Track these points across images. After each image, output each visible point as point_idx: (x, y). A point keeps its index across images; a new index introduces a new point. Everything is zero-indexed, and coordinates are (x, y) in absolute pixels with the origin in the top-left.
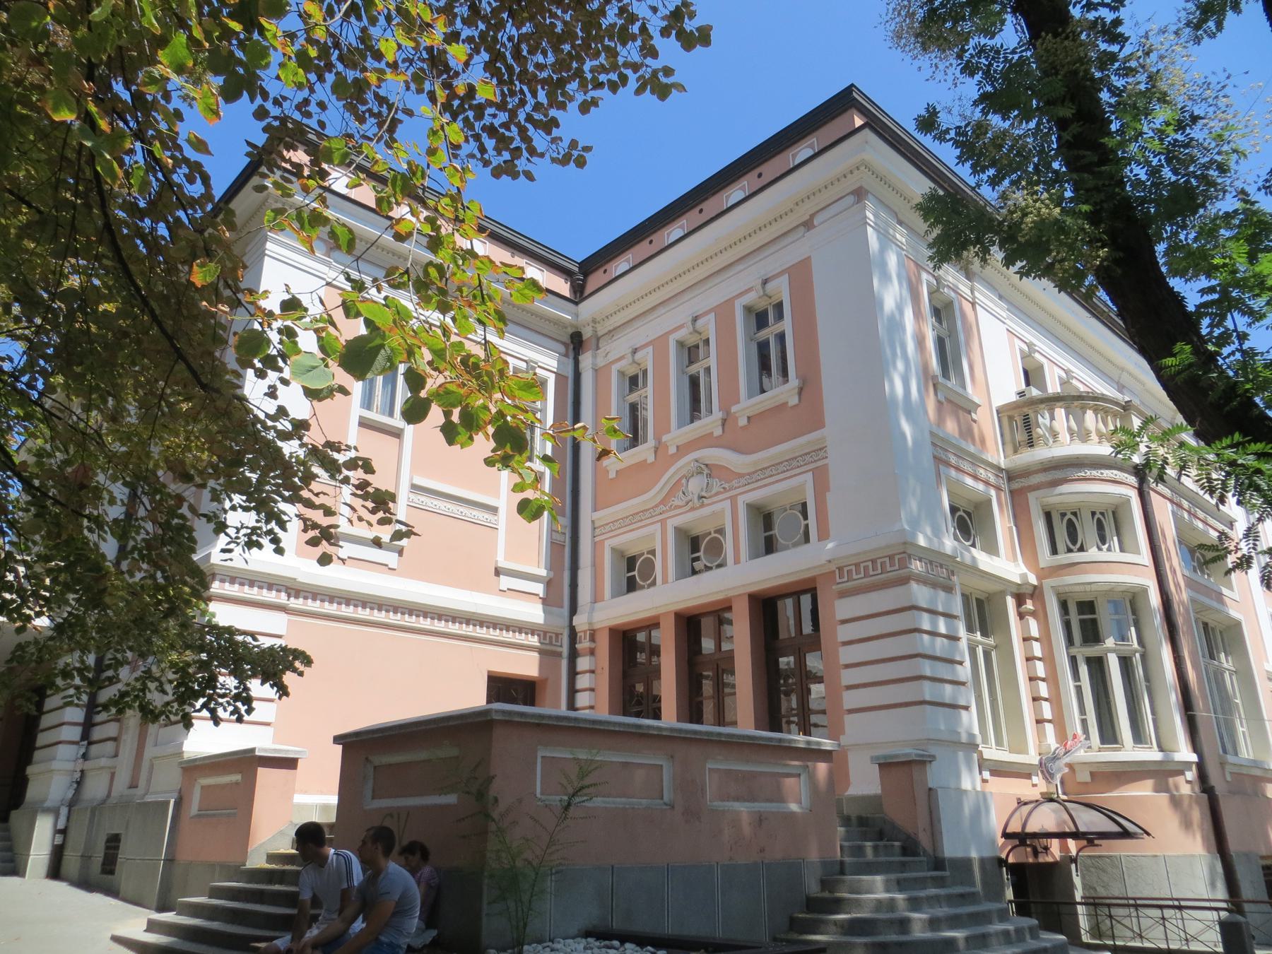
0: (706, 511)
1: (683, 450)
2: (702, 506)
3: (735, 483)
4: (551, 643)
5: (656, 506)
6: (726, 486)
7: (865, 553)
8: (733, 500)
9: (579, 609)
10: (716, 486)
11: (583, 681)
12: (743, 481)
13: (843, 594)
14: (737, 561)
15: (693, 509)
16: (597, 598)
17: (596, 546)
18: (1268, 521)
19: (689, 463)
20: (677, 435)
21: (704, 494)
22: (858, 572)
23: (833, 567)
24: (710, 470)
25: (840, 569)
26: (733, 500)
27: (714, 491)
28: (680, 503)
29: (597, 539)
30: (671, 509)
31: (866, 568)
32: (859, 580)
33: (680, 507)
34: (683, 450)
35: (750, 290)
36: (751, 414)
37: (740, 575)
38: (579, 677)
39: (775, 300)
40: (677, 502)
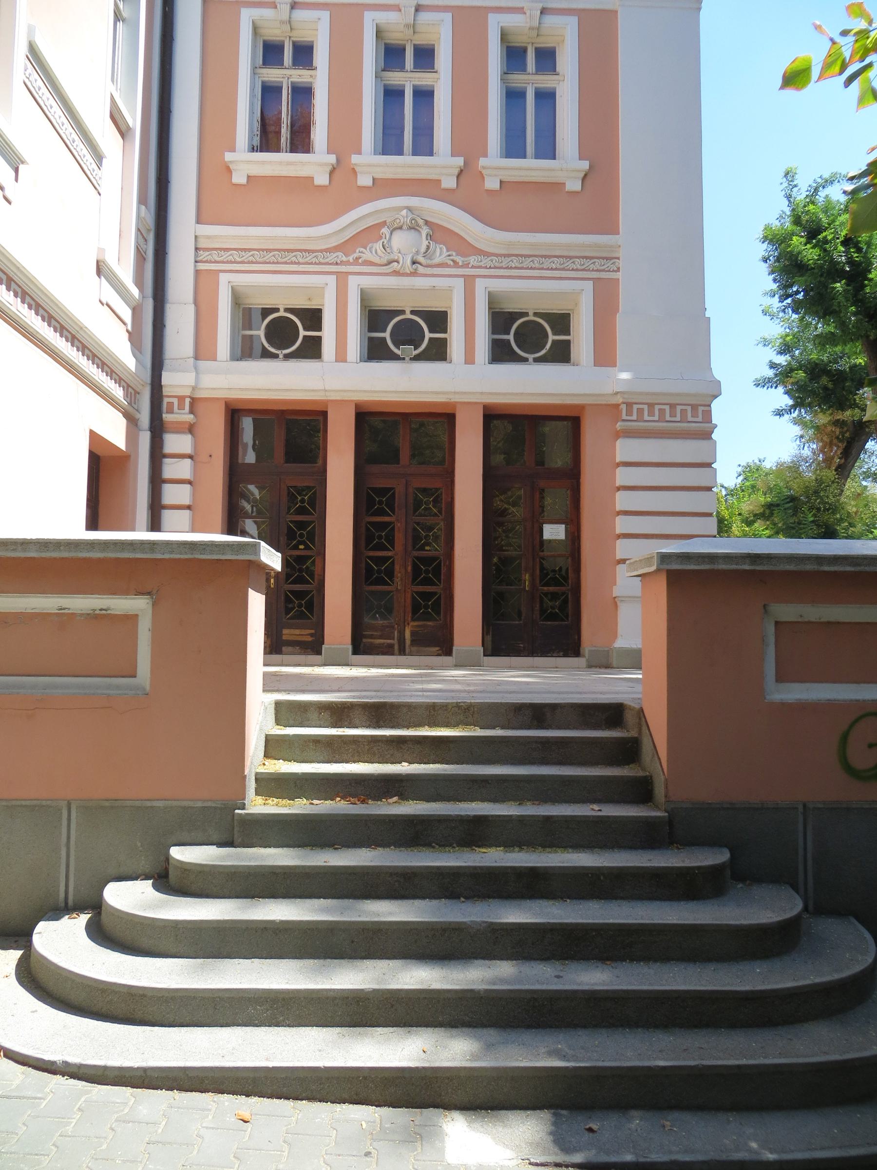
0: (419, 282)
1: (384, 187)
2: (414, 274)
3: (473, 260)
4: (661, 419)
5: (327, 250)
6: (459, 260)
7: (688, 395)
8: (342, 280)
9: (167, 363)
10: (440, 254)
11: (172, 469)
12: (486, 261)
13: (629, 434)
14: (469, 359)
15: (396, 273)
16: (203, 350)
17: (204, 282)
18: (876, 453)
19: (402, 208)
20: (370, 163)
21: (420, 259)
22: (651, 413)
23: (619, 400)
24: (437, 232)
25: (629, 405)
26: (469, 282)
27: (437, 260)
28: (376, 260)
29: (202, 266)
30: (356, 261)
31: (640, 411)
32: (651, 422)
33: (372, 264)
34: (384, 187)
35: (397, 8)
36: (505, 179)
37: (466, 379)
38: (166, 461)
39: (422, 40)
40: (367, 255)
